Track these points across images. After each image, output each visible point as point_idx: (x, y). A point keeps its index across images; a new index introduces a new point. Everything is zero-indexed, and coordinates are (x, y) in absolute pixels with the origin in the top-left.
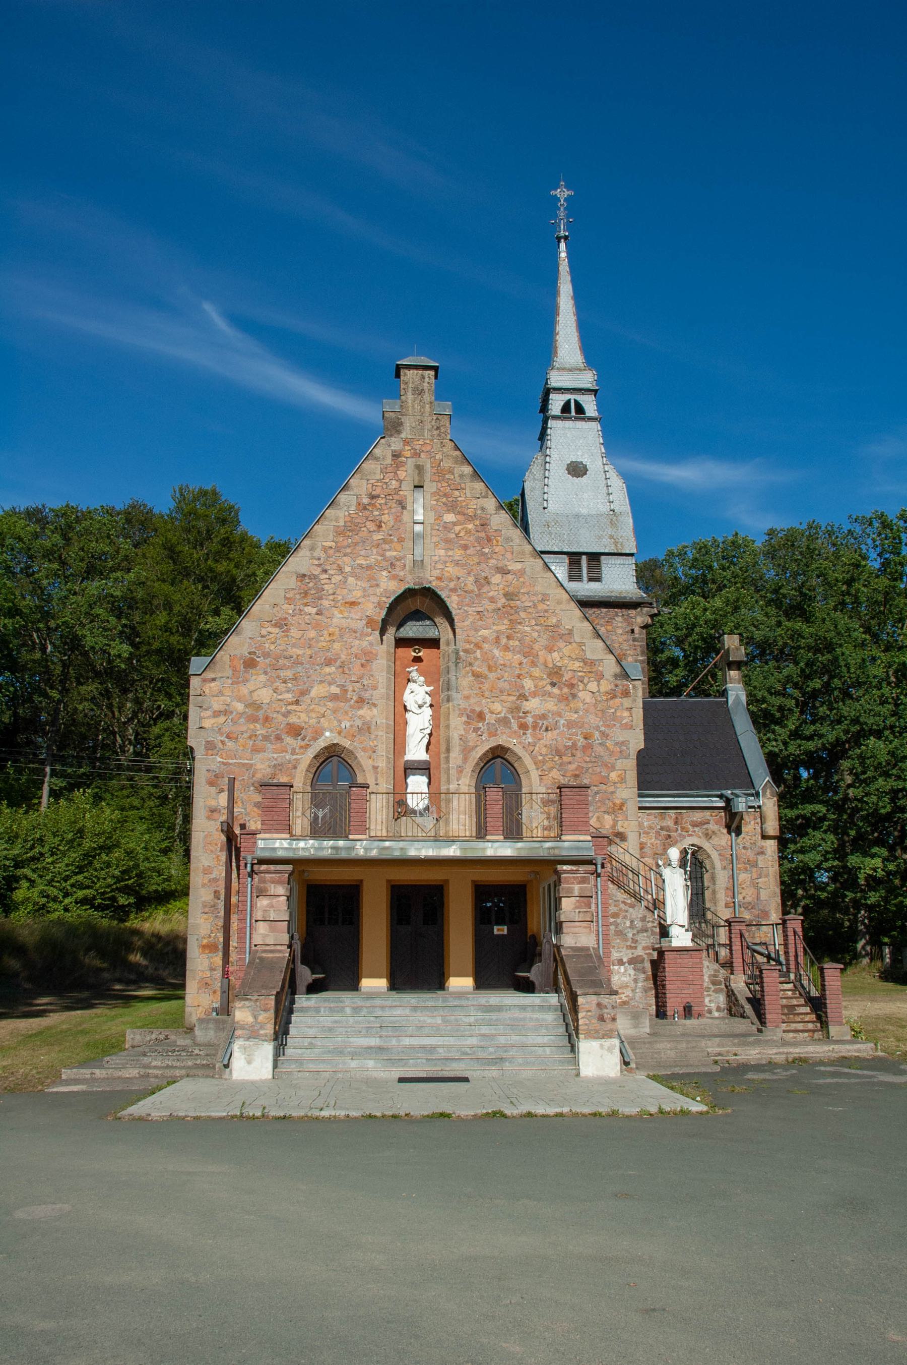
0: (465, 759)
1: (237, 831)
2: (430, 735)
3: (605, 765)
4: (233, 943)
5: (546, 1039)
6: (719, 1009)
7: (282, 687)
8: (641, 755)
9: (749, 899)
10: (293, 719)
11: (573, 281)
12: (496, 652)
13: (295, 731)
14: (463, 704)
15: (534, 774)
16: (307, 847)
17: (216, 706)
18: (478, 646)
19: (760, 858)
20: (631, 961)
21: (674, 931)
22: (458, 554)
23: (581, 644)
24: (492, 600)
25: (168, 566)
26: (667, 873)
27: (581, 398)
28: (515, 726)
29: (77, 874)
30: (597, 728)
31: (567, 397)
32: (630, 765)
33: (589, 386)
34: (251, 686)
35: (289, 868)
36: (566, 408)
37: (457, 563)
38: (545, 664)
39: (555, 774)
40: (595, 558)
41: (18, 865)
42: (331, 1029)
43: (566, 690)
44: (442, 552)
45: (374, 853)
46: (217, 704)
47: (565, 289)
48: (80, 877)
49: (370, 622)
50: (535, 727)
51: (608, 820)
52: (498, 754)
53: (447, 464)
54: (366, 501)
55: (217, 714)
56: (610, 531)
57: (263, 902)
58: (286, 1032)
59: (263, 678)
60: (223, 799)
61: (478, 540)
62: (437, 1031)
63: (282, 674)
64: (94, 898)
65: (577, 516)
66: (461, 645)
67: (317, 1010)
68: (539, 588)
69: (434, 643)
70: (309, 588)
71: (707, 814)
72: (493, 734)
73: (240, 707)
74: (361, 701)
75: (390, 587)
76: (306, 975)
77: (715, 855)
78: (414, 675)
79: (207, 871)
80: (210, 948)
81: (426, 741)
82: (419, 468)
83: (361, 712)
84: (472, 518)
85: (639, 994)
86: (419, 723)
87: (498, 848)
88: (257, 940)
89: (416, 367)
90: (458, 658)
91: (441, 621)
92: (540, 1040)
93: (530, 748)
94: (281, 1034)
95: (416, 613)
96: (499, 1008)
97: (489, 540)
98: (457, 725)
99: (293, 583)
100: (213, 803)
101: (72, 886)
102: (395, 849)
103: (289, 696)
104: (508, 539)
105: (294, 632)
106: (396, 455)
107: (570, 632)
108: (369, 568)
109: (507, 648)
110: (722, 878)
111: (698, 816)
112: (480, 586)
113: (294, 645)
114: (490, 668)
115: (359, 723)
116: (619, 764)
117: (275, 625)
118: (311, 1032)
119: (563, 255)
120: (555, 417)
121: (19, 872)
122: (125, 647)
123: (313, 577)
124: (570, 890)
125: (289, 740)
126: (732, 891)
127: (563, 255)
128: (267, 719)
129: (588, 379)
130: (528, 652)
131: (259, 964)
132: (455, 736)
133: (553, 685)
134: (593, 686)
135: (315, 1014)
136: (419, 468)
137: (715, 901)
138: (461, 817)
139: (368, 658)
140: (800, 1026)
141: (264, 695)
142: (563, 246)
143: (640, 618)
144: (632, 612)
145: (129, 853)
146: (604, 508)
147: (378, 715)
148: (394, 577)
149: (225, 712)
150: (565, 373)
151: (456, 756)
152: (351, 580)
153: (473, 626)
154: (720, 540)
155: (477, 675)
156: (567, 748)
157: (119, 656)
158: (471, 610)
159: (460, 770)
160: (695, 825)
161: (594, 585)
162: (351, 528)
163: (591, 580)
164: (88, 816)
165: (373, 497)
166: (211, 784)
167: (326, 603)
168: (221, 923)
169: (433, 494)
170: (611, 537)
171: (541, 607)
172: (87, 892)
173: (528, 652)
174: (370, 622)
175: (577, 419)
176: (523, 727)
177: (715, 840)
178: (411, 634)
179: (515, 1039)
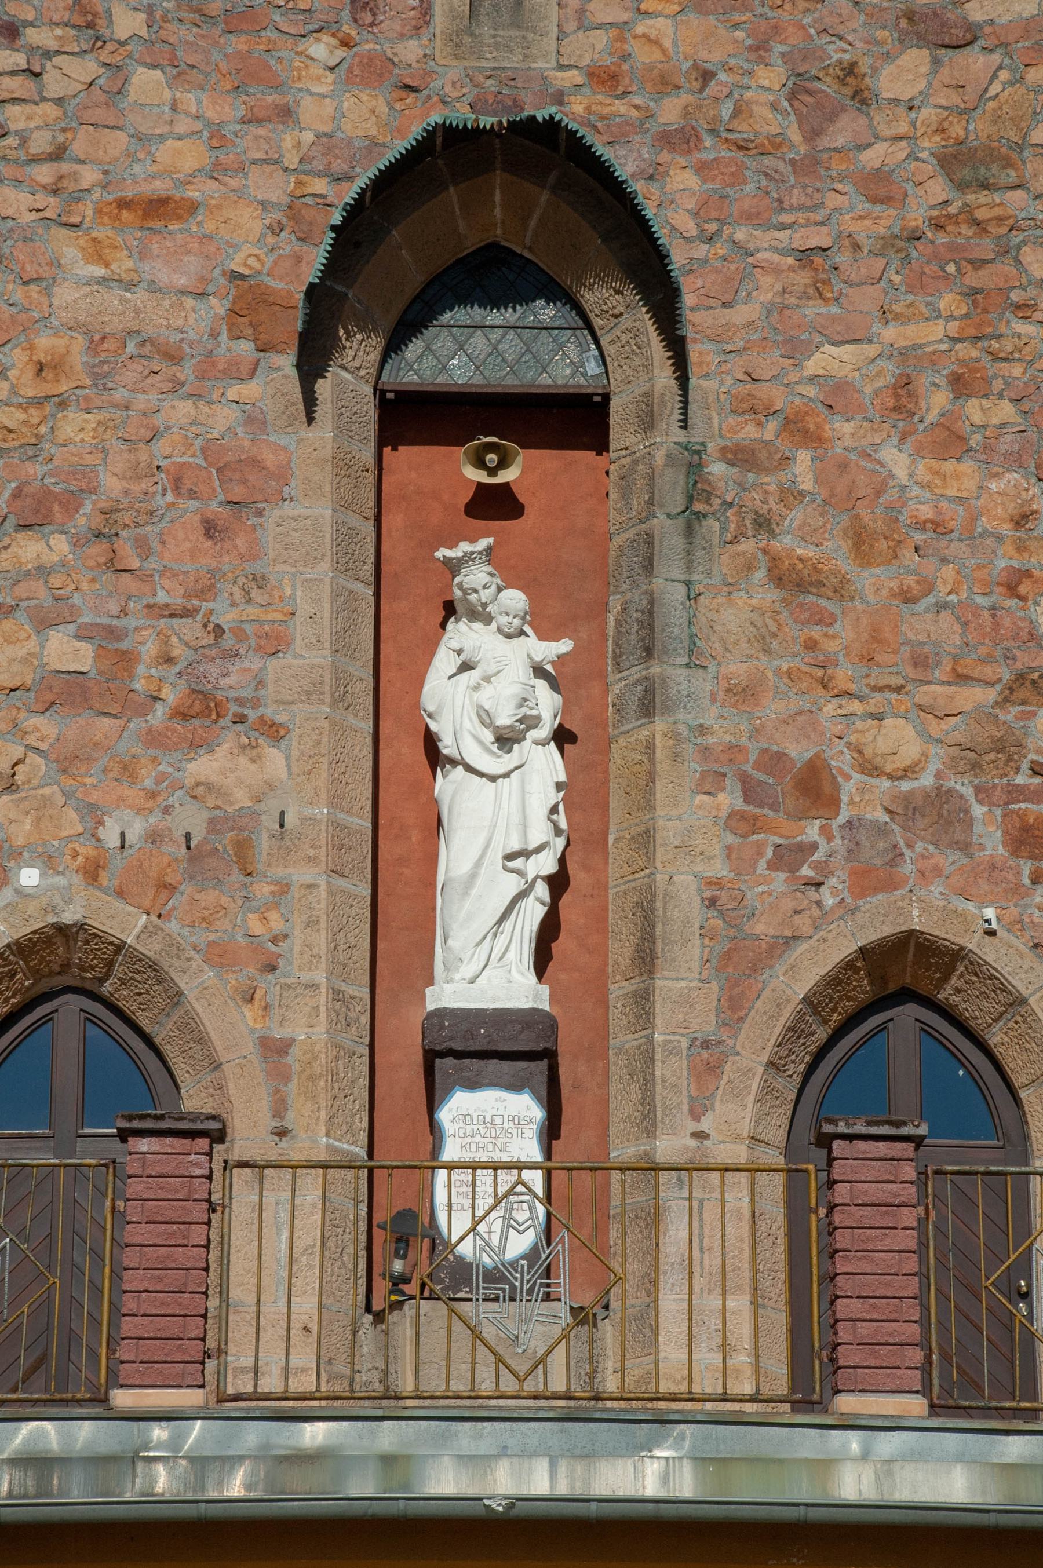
0: (734, 1007)
2: (558, 883)
12: (897, 461)
14: (724, 727)
18: (800, 429)
24: (880, 188)
28: (991, 838)
49: (248, 304)
52: (902, 982)
66: (716, 425)
72: (874, 878)
74: (204, 711)
75: (351, 123)
78: (477, 577)
81: (533, 912)
83: (202, 767)
86: (499, 820)
91: (608, 299)
98: (692, 833)
109: (950, 441)
114: (862, 543)
115: (192, 819)
132: (682, 886)
138: (710, 1303)
139: (236, 494)
147: (292, 781)
148: (371, 71)
151: (685, 989)
152: (146, 81)
155: (794, 580)
159: (708, 1060)
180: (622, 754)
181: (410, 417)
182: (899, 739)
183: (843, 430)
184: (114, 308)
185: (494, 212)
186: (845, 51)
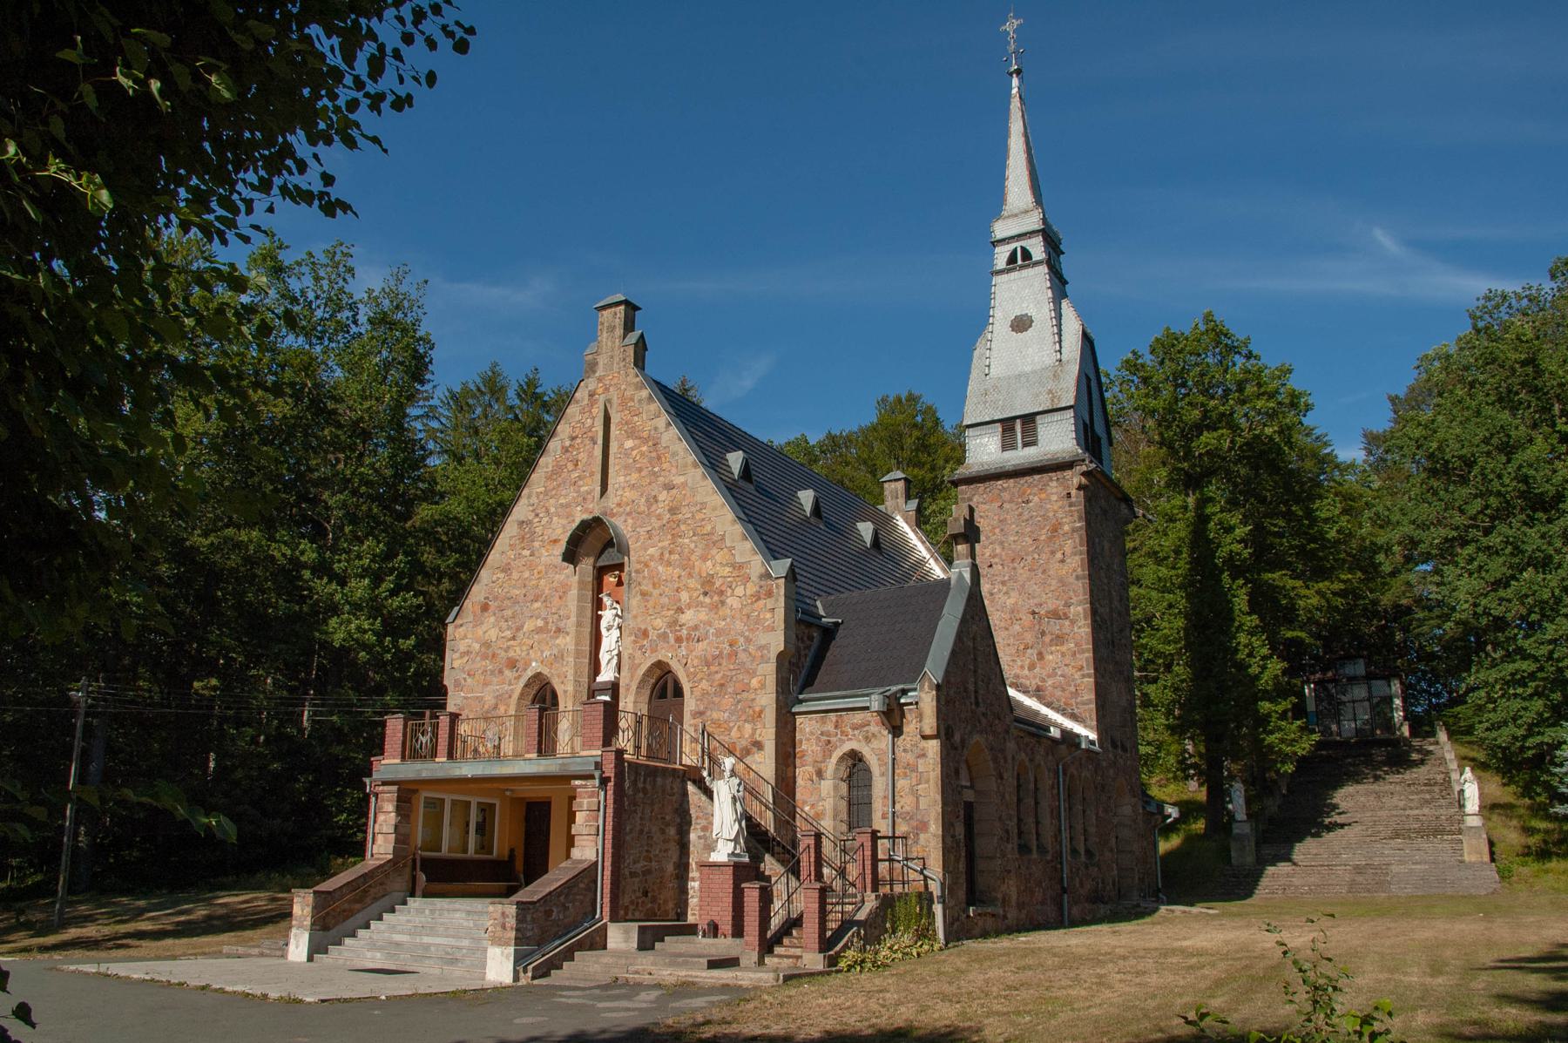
2: (619, 655)
7: (504, 625)
8: (780, 656)
9: (907, 808)
10: (511, 654)
13: (512, 664)
19: (920, 761)
22: (634, 477)
24: (659, 517)
28: (672, 641)
30: (742, 634)
34: (484, 628)
36: (1012, 259)
39: (704, 685)
40: (1029, 419)
43: (716, 598)
46: (462, 647)
54: (567, 443)
59: (492, 619)
72: (654, 650)
74: (559, 630)
81: (615, 661)
84: (645, 441)
97: (659, 458)
104: (675, 454)
105: (515, 575)
106: (591, 395)
107: (723, 538)
109: (669, 564)
113: (514, 587)
115: (555, 651)
119: (1015, 91)
123: (530, 522)
125: (507, 673)
130: (687, 566)
133: (706, 594)
134: (739, 591)
139: (563, 592)
141: (493, 634)
142: (1015, 81)
143: (1074, 478)
144: (1068, 474)
155: (643, 594)
158: (642, 531)
161: (1031, 450)
162: (558, 470)
163: (1025, 445)
165: (573, 439)
167: (536, 544)
171: (699, 516)
173: (687, 566)
175: (1027, 266)
177: (875, 744)
182: (659, 622)
186: (1495, 727)
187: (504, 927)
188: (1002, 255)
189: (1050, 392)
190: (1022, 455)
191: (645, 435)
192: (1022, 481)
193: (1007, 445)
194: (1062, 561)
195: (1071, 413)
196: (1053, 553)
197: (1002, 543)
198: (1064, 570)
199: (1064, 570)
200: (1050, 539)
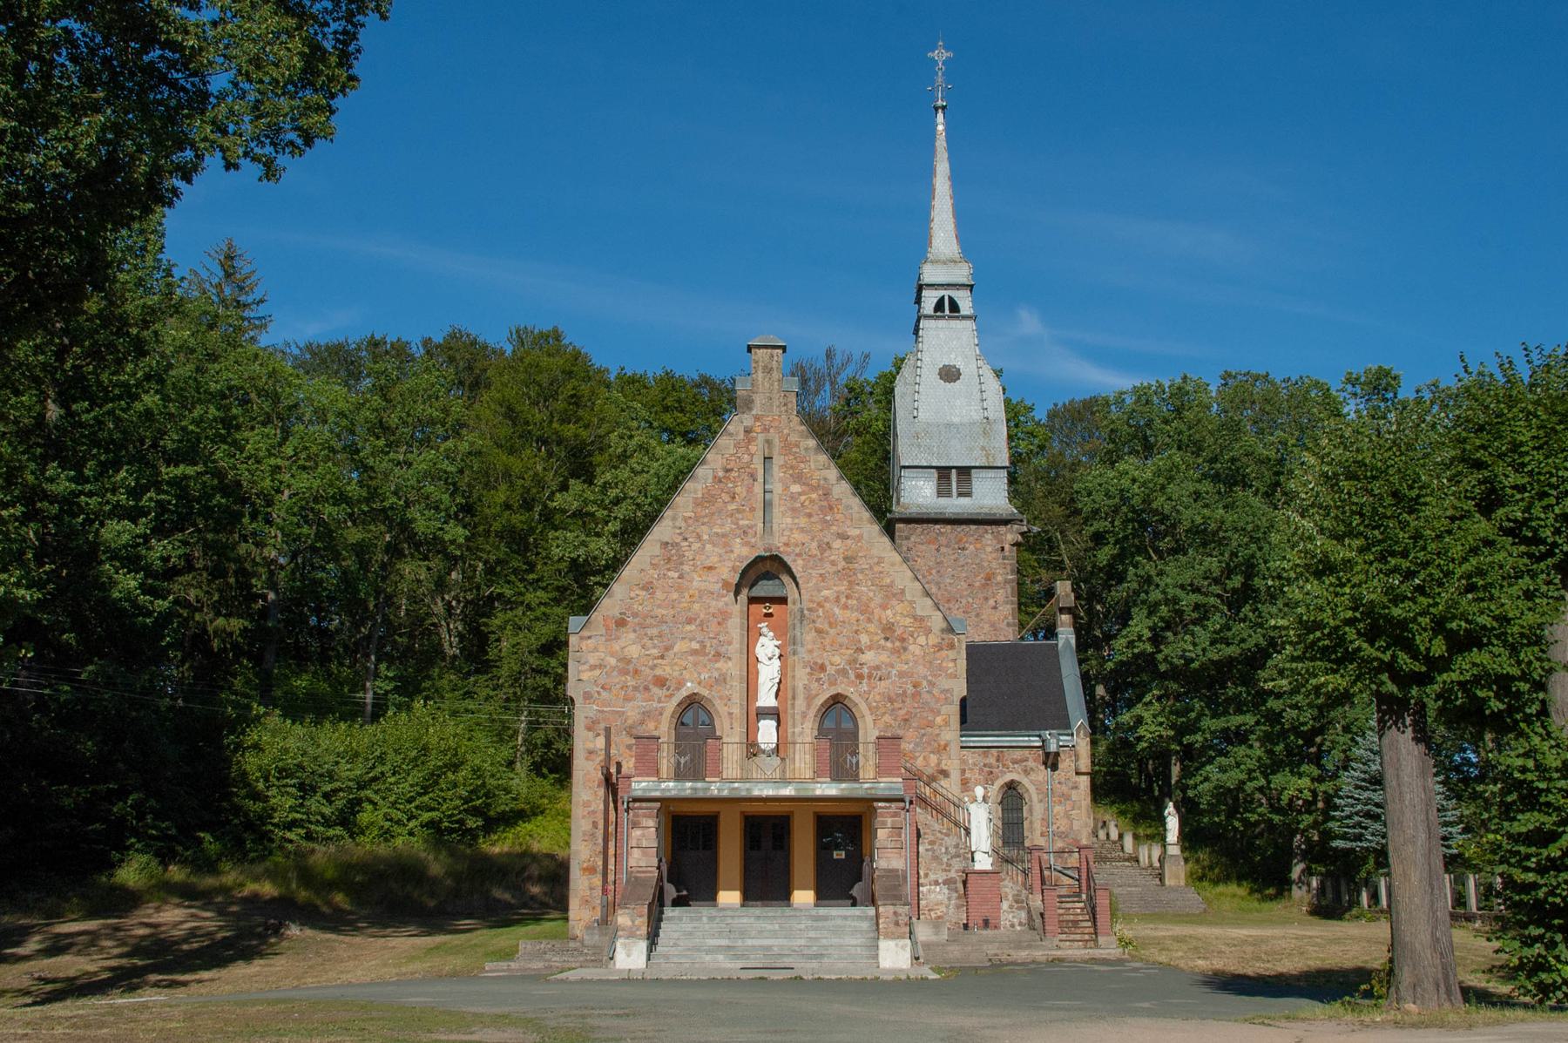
0: (809, 706)
1: (613, 770)
3: (932, 710)
4: (611, 867)
5: (859, 942)
6: (1020, 924)
9: (1062, 829)
10: (658, 672)
11: (950, 159)
12: (837, 610)
13: (661, 682)
14: (807, 657)
15: (869, 719)
16: (671, 788)
17: (592, 661)
18: (820, 605)
20: (945, 883)
21: (977, 856)
22: (803, 521)
23: (911, 602)
24: (833, 563)
25: (505, 430)
26: (973, 808)
27: (956, 294)
28: (852, 677)
29: (420, 795)
30: (925, 677)
31: (941, 293)
32: (955, 709)
33: (965, 281)
34: (622, 642)
35: (658, 805)
36: (939, 306)
37: (802, 530)
38: (880, 620)
39: (887, 718)
40: (965, 472)
41: (361, 786)
42: (691, 934)
43: (898, 644)
44: (789, 520)
45: (725, 793)
46: (593, 659)
47: (942, 167)
48: (426, 798)
49: (726, 584)
50: (870, 677)
51: (933, 759)
52: (837, 701)
53: (793, 438)
54: (721, 474)
55: (593, 668)
56: (982, 441)
57: (637, 833)
58: (657, 935)
59: (632, 636)
60: (600, 742)
61: (821, 508)
62: (774, 934)
63: (650, 632)
64: (441, 821)
65: (949, 425)
66: (806, 604)
67: (680, 919)
68: (875, 552)
69: (783, 601)
70: (672, 555)
71: (1026, 752)
73: (613, 661)
74: (718, 655)
75: (743, 553)
76: (671, 891)
77: (1032, 789)
78: (765, 630)
79: (587, 804)
80: (591, 870)
82: (768, 442)
83: (718, 665)
84: (814, 489)
85: (952, 910)
86: (769, 673)
87: (828, 789)
88: (632, 863)
89: (766, 347)
90: (803, 615)
91: (786, 578)
92: (854, 942)
93: (865, 697)
94: (653, 937)
95: (764, 578)
96: (825, 918)
97: (831, 508)
98: (801, 676)
99: (657, 550)
100: (590, 746)
101: (417, 807)
102: (742, 789)
103: (655, 652)
104: (848, 507)
105: (659, 595)
106: (748, 431)
107: (903, 592)
108: (724, 536)
109: (846, 607)
110: (1038, 809)
111: (1018, 754)
112: (822, 551)
113: (659, 606)
114: (831, 625)
115: (716, 674)
116: (944, 710)
117: (643, 589)
118: (676, 935)
119: (940, 128)
120: (928, 317)
121: (363, 794)
122: (460, 530)
124: (884, 823)
125: (655, 690)
126: (1046, 821)
127: (940, 128)
128: (636, 672)
129: (962, 273)
130: (865, 609)
131: (635, 882)
132: (800, 685)
133: (887, 639)
134: (922, 640)
135: (677, 922)
136: (768, 442)
137: (1032, 830)
138: (803, 760)
139: (724, 616)
140: (1078, 937)
141: (634, 651)
142: (940, 116)
143: (1011, 535)
144: (1002, 529)
145: (476, 771)
146: (977, 416)
147: (733, 668)
148: (747, 544)
149: (600, 666)
150: (940, 266)
151: (800, 703)
152: (709, 547)
153: (812, 586)
154: (1167, 384)
155: (819, 631)
156: (898, 695)
157: (453, 542)
159: (804, 715)
160: (1015, 762)
161: (964, 501)
162: (708, 499)
163: (960, 495)
164: (431, 730)
165: (727, 471)
166: (589, 729)
167: (686, 568)
168: (600, 848)
169: (781, 467)
170: (983, 448)
171: (876, 569)
172: (434, 814)
173: (865, 609)
174: (726, 584)
176: (860, 677)
177: (1033, 776)
178: (762, 594)
179: (835, 941)
180: (790, 661)
181: (752, 600)
183: (827, 605)
184: (703, 586)
185: (768, 566)
187: (897, 924)
188: (930, 299)
189: (983, 448)
190: (956, 505)
191: (814, 482)
192: (959, 528)
193: (943, 491)
194: (995, 608)
195: (1004, 473)
196: (986, 599)
197: (938, 584)
198: (996, 616)
199: (996, 616)
200: (984, 586)
